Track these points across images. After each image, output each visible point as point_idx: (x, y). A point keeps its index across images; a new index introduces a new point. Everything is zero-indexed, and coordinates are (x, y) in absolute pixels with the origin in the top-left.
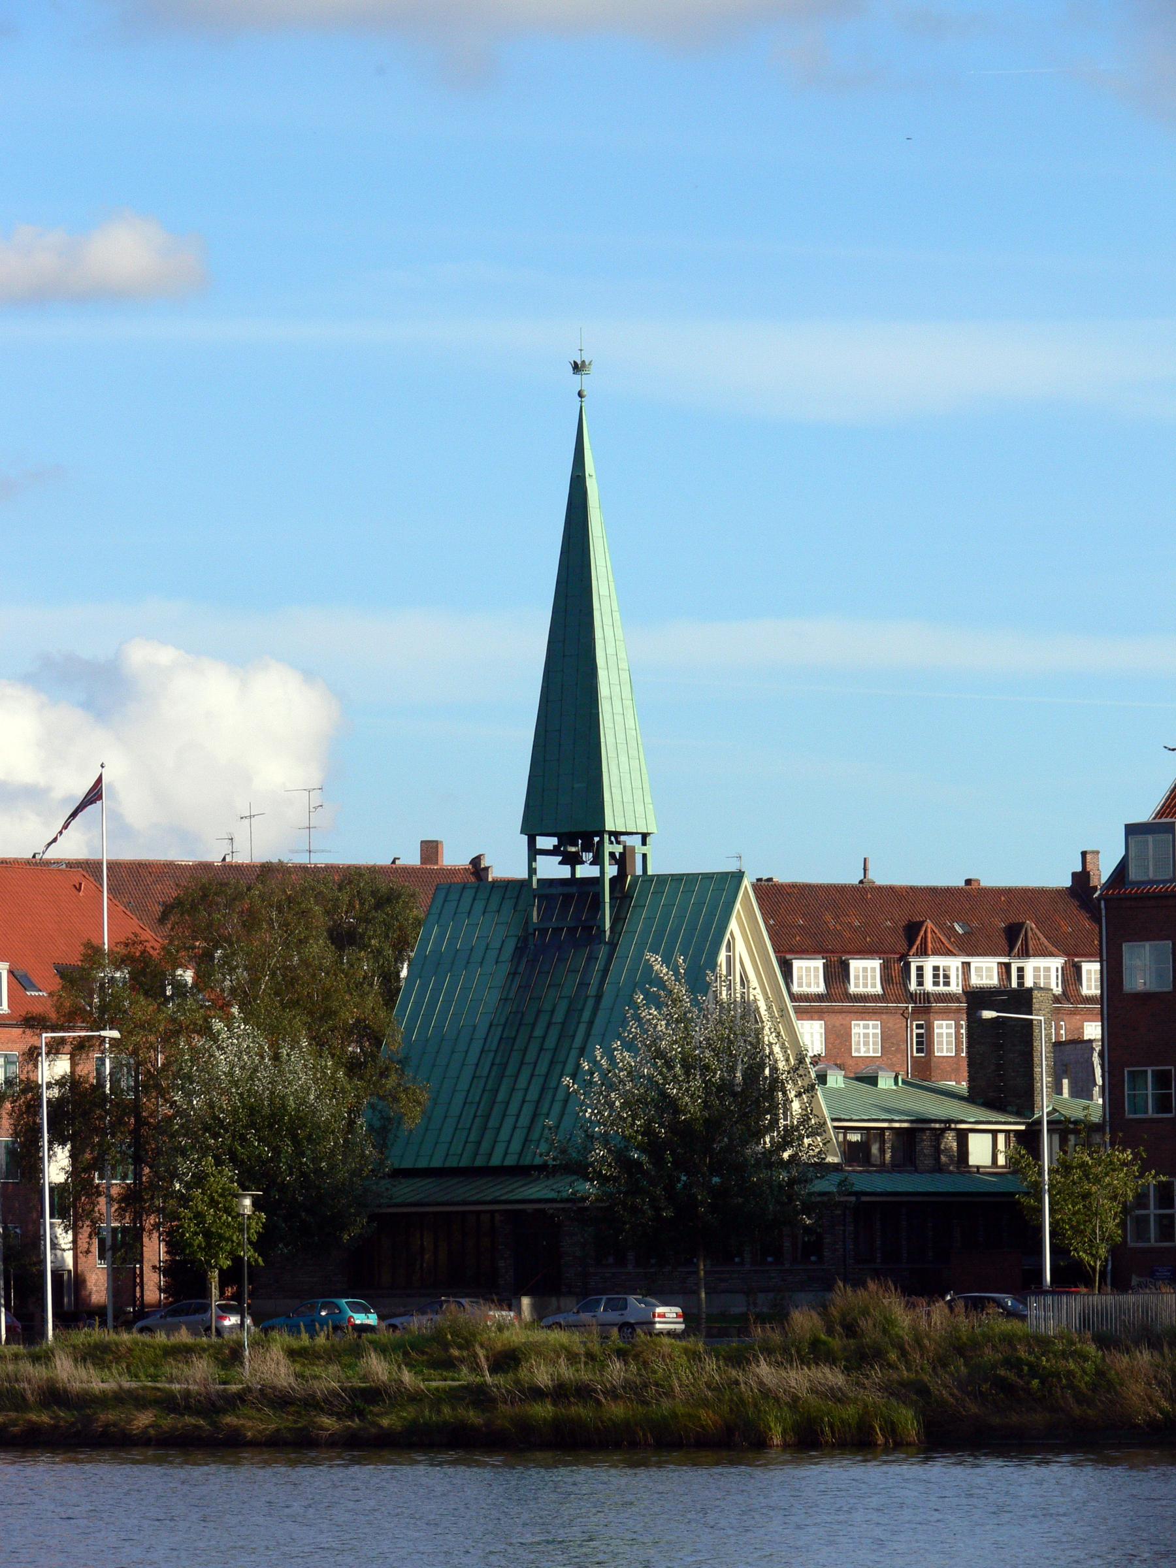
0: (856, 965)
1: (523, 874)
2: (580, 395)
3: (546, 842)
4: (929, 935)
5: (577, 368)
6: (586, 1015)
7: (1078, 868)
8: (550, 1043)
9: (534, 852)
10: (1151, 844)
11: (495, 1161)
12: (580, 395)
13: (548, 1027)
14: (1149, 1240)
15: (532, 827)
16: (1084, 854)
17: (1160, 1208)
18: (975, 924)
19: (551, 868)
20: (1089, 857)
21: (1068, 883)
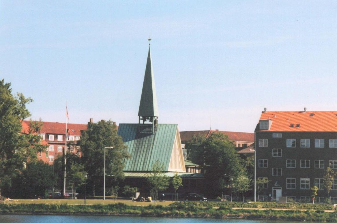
0: (59, 136)
1: (138, 123)
2: (150, 44)
3: (141, 117)
4: (70, 132)
5: (149, 40)
6: (151, 146)
7: (89, 121)
8: (145, 150)
9: (140, 119)
10: (264, 123)
11: (138, 170)
12: (150, 44)
13: (144, 149)
14: (262, 187)
15: (139, 115)
16: (91, 119)
17: (290, 182)
18: (75, 130)
19: (142, 122)
20: (91, 120)
21: (87, 124)
